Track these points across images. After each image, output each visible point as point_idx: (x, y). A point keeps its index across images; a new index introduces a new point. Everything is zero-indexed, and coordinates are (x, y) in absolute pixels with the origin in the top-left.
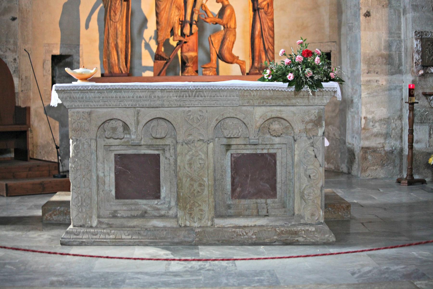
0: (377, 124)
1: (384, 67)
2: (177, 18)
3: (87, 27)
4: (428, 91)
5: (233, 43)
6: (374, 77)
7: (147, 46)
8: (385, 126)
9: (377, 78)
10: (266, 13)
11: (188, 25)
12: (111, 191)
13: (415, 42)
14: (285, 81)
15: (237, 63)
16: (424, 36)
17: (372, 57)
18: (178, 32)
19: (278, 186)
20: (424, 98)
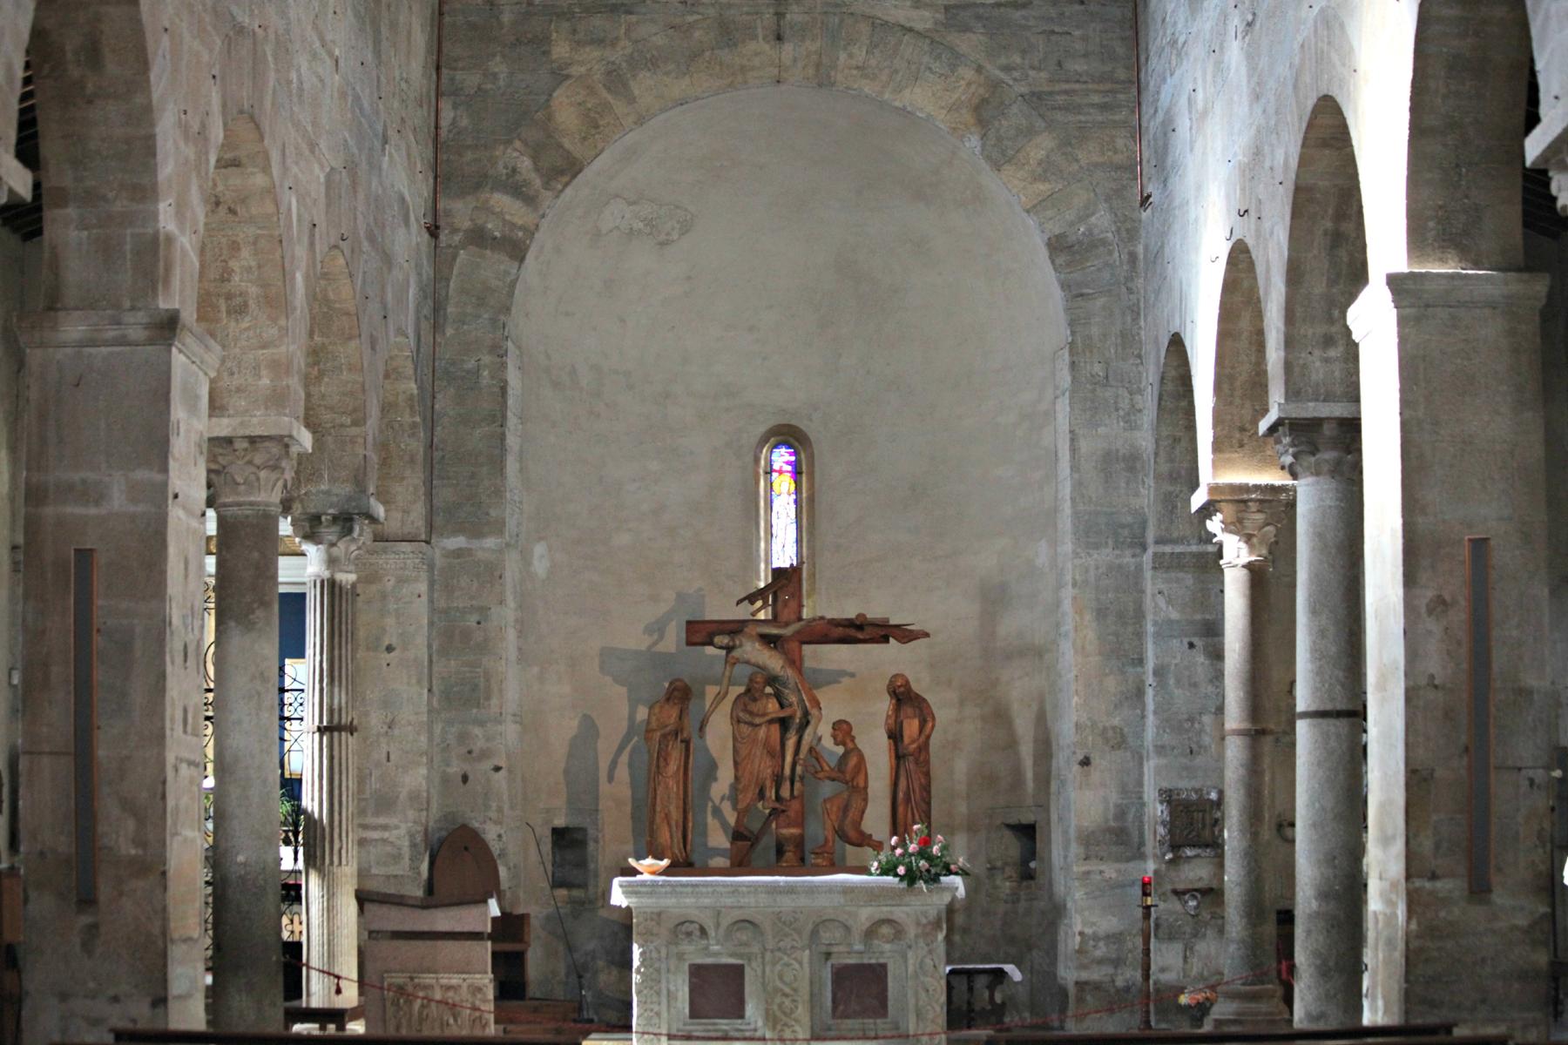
0: (1101, 944)
1: (1114, 848)
2: (769, 771)
3: (611, 778)
4: (1181, 887)
5: (863, 812)
6: (1093, 866)
7: (717, 812)
8: (1115, 947)
9: (1103, 868)
10: (917, 762)
11: (788, 783)
12: (684, 1008)
13: (1159, 808)
14: (896, 875)
15: (869, 845)
16: (1175, 797)
17: (1093, 832)
18: (771, 793)
19: (890, 1003)
20: (1175, 898)
